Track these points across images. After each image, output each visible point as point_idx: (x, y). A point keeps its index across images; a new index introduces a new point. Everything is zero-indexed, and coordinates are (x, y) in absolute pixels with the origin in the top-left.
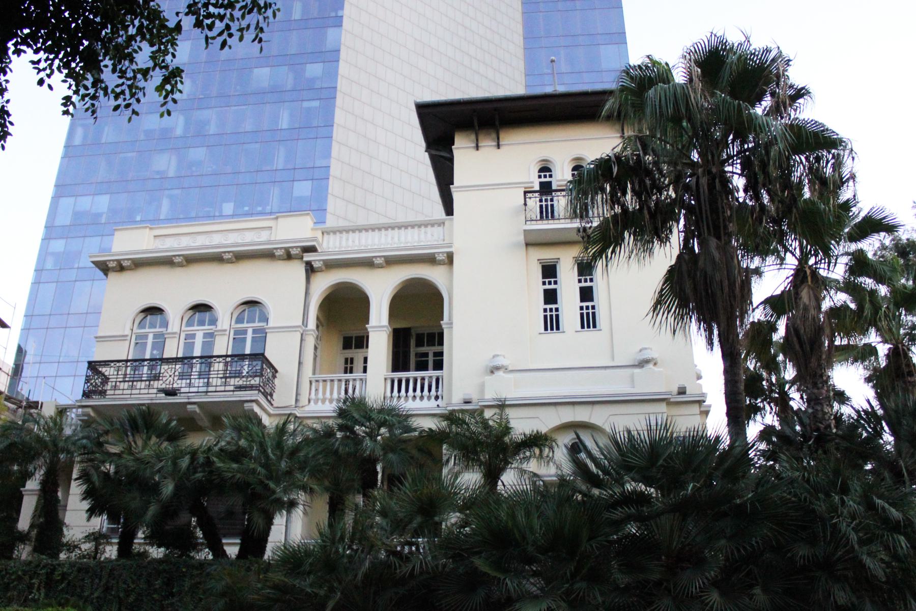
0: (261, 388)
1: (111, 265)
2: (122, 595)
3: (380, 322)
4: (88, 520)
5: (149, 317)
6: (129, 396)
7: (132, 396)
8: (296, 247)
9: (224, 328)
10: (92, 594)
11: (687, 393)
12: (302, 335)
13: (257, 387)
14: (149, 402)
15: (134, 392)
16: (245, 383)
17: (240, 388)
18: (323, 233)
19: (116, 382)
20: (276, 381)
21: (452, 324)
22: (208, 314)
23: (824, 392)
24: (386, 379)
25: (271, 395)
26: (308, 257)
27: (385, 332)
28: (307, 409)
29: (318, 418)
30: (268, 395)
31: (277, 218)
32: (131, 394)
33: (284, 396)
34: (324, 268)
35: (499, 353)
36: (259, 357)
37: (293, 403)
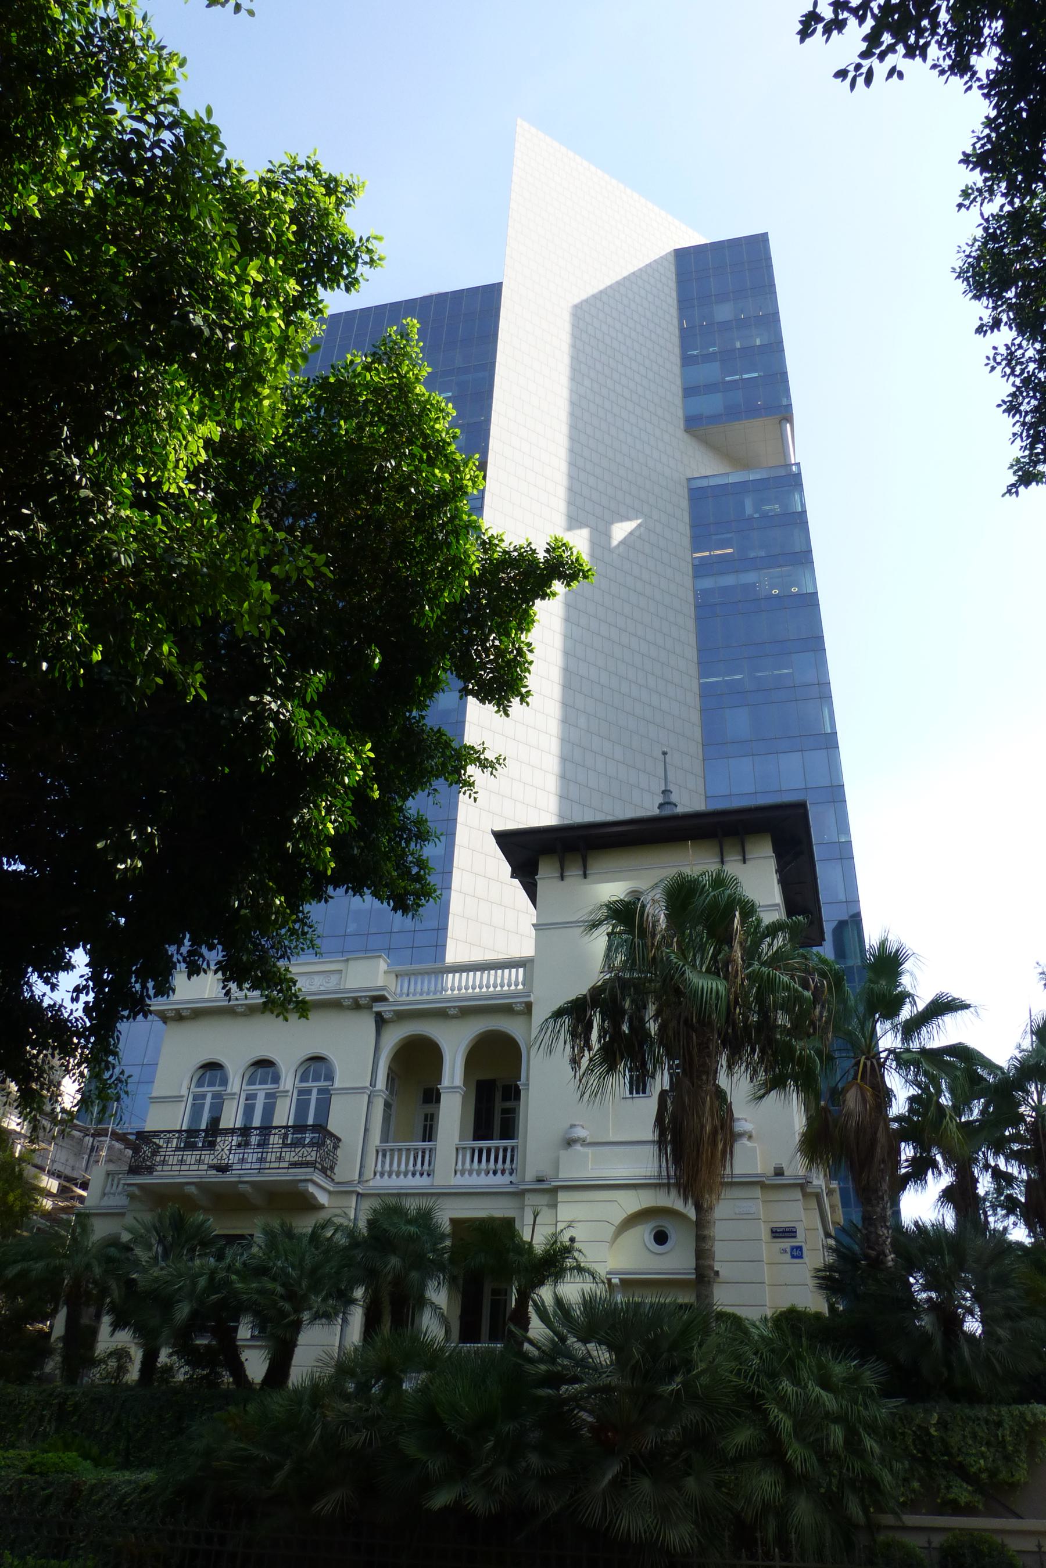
0: (317, 1165)
1: (170, 1014)
2: (131, 1430)
3: (453, 1083)
4: (112, 1335)
5: (208, 1074)
6: (177, 1173)
7: (182, 1173)
8: (365, 997)
9: (287, 1088)
10: (102, 1428)
11: (786, 1174)
12: (369, 1096)
13: (312, 1164)
14: (198, 1180)
15: (183, 1167)
16: (300, 1159)
17: (294, 1165)
18: (397, 976)
19: (165, 1156)
20: (339, 1152)
21: (528, 1085)
22: (271, 1070)
23: (878, 1209)
24: (457, 1149)
25: (332, 1169)
26: (378, 1007)
27: (458, 1094)
28: (371, 1183)
29: (379, 1195)
30: (327, 1171)
31: (347, 960)
32: (260, 1169)
33: (347, 1168)
34: (395, 1018)
35: (577, 1123)
36: (320, 1127)
37: (357, 1177)
